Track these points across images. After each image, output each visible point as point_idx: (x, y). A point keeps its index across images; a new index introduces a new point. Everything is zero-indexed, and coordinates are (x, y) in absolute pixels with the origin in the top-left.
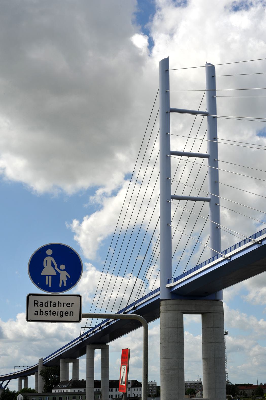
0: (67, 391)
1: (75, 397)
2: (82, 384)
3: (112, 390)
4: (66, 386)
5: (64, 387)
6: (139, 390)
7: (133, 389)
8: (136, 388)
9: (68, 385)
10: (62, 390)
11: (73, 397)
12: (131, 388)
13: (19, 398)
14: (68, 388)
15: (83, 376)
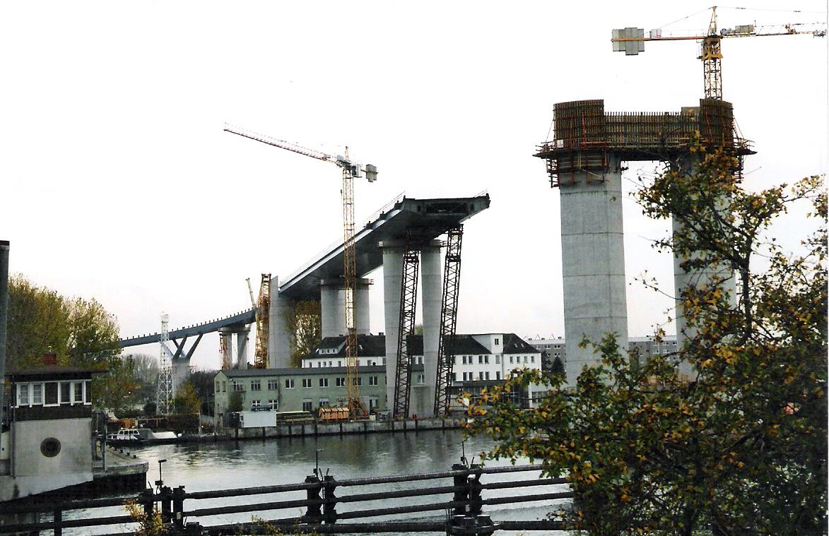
0: (358, 362)
1: (309, 381)
2: (373, 345)
3: (470, 361)
4: (336, 352)
5: (331, 352)
6: (522, 359)
7: (507, 357)
8: (515, 356)
9: (341, 347)
10: (327, 361)
11: (371, 378)
12: (502, 354)
13: (218, 382)
14: (342, 354)
15: (377, 324)
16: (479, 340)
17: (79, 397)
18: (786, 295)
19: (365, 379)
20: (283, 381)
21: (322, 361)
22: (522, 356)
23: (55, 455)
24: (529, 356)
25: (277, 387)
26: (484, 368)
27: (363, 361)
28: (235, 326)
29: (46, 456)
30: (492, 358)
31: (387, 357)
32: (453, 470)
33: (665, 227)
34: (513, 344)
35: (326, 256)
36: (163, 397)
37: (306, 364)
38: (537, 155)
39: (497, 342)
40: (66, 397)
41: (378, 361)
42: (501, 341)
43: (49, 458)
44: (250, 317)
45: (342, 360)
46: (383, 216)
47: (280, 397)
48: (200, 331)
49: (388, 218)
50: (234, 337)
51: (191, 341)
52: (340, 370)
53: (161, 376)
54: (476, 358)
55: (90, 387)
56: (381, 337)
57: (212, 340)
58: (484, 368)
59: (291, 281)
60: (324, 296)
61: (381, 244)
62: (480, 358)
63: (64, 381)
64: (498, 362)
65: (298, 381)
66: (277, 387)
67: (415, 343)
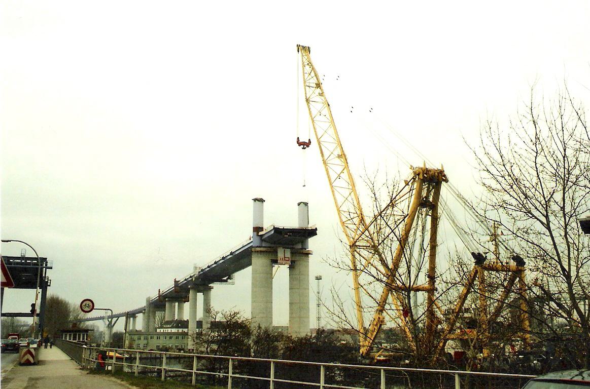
2: (185, 324)
5: (168, 326)
15: (186, 316)
17: (83, 339)
19: (162, 337)
20: (149, 337)
21: (165, 329)
25: (147, 339)
27: (180, 330)
28: (131, 315)
31: (189, 329)
32: (197, 370)
36: (103, 341)
37: (158, 330)
40: (79, 339)
41: (186, 330)
44: (140, 311)
45: (172, 329)
46: (215, 263)
47: (148, 343)
48: (118, 316)
49: (234, 254)
50: (132, 319)
51: (114, 319)
52: (168, 334)
53: (101, 334)
56: (188, 321)
57: (123, 320)
59: (236, 251)
60: (167, 305)
61: (189, 287)
63: (275, 360)
65: (155, 337)
66: (147, 339)
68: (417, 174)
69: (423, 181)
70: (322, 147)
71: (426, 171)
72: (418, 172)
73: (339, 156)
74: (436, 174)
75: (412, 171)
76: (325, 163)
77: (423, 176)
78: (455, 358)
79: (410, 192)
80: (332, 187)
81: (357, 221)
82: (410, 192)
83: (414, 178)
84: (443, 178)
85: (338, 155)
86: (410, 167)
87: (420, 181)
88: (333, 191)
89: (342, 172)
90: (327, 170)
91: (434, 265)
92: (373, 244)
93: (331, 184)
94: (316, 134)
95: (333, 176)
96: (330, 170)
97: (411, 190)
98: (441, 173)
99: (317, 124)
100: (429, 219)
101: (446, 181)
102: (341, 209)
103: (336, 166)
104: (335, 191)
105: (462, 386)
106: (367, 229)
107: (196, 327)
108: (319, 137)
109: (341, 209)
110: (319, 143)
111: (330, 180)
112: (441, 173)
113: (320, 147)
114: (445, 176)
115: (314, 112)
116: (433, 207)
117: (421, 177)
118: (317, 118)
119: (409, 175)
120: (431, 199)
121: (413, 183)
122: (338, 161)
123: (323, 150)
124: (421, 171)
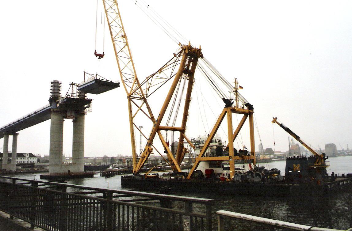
3: (25, 159)
6: (33, 159)
7: (30, 158)
8: (31, 158)
16: (24, 155)
18: (323, 168)
22: (33, 158)
23: (328, 144)
24: (34, 158)
26: (24, 160)
29: (335, 146)
30: (26, 158)
33: (171, 147)
34: (31, 155)
35: (228, 87)
38: (91, 100)
39: (28, 155)
42: (29, 155)
43: (337, 146)
54: (23, 158)
55: (232, 146)
58: (24, 160)
62: (31, 159)
64: (27, 159)
67: (10, 155)
68: (184, 49)
69: (186, 55)
70: (111, 29)
71: (190, 48)
72: (184, 48)
73: (123, 36)
74: (196, 51)
75: (180, 47)
76: (113, 39)
77: (188, 51)
78: (213, 199)
79: (174, 62)
80: (117, 56)
81: (132, 80)
82: (174, 62)
83: (181, 52)
84: (200, 54)
85: (122, 35)
86: (179, 43)
87: (185, 55)
88: (117, 60)
89: (124, 47)
90: (114, 45)
91: (187, 114)
92: (143, 96)
93: (116, 54)
94: (108, 20)
95: (118, 50)
96: (108, 16)
97: (176, 61)
98: (199, 50)
99: (113, 29)
100: (187, 81)
101: (202, 57)
102: (122, 72)
103: (120, 44)
104: (115, 44)
105: (221, 230)
106: (140, 87)
107: (7, 156)
108: (110, 22)
109: (122, 72)
110: (110, 27)
111: (120, 69)
112: (199, 50)
113: (110, 29)
114: (201, 53)
115: (107, 7)
116: (191, 74)
117: (187, 51)
118: (109, 10)
119: (178, 49)
120: (190, 69)
121: (179, 56)
122: (121, 39)
123: (135, 134)
124: (187, 47)
